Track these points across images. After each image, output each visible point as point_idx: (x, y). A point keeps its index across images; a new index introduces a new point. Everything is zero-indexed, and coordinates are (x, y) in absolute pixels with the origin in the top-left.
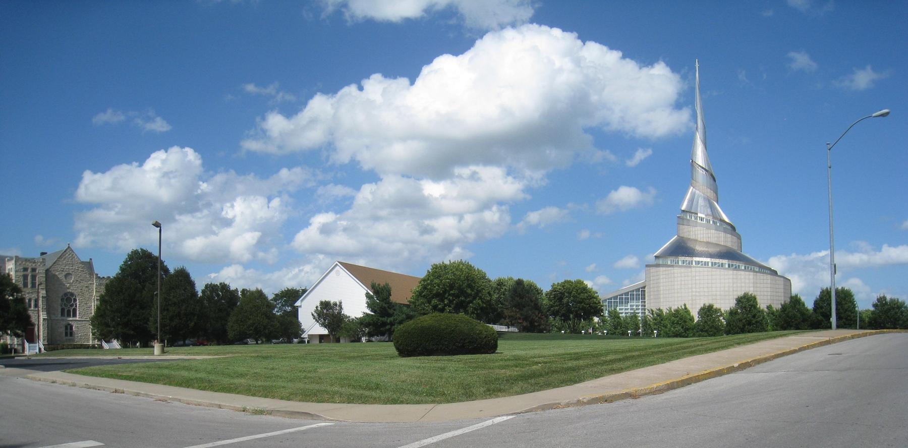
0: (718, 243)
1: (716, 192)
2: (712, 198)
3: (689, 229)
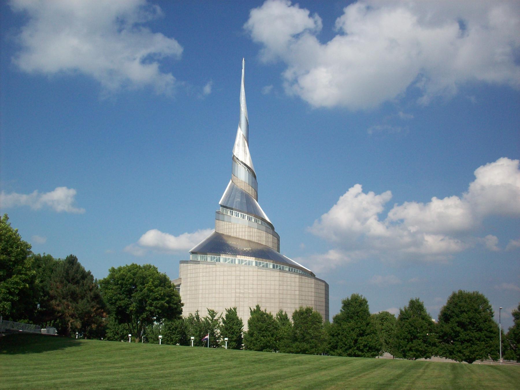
0: (260, 243)
1: (256, 191)
2: (253, 196)
3: (230, 226)
